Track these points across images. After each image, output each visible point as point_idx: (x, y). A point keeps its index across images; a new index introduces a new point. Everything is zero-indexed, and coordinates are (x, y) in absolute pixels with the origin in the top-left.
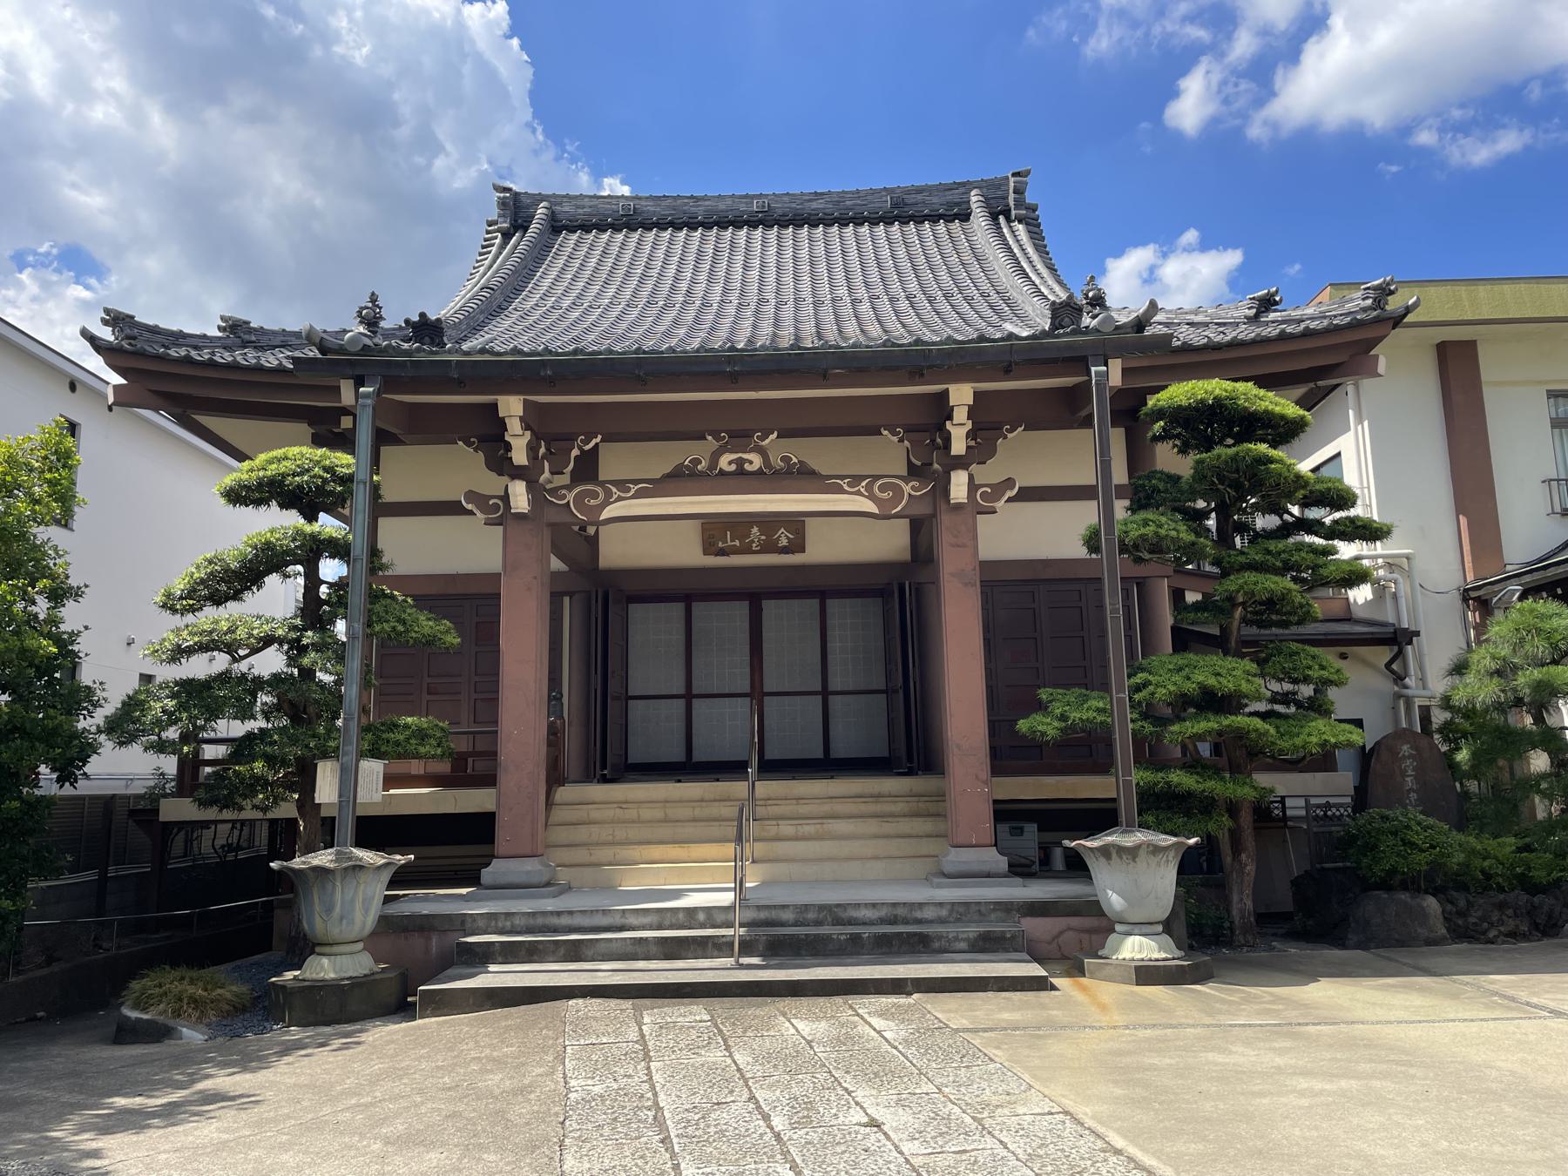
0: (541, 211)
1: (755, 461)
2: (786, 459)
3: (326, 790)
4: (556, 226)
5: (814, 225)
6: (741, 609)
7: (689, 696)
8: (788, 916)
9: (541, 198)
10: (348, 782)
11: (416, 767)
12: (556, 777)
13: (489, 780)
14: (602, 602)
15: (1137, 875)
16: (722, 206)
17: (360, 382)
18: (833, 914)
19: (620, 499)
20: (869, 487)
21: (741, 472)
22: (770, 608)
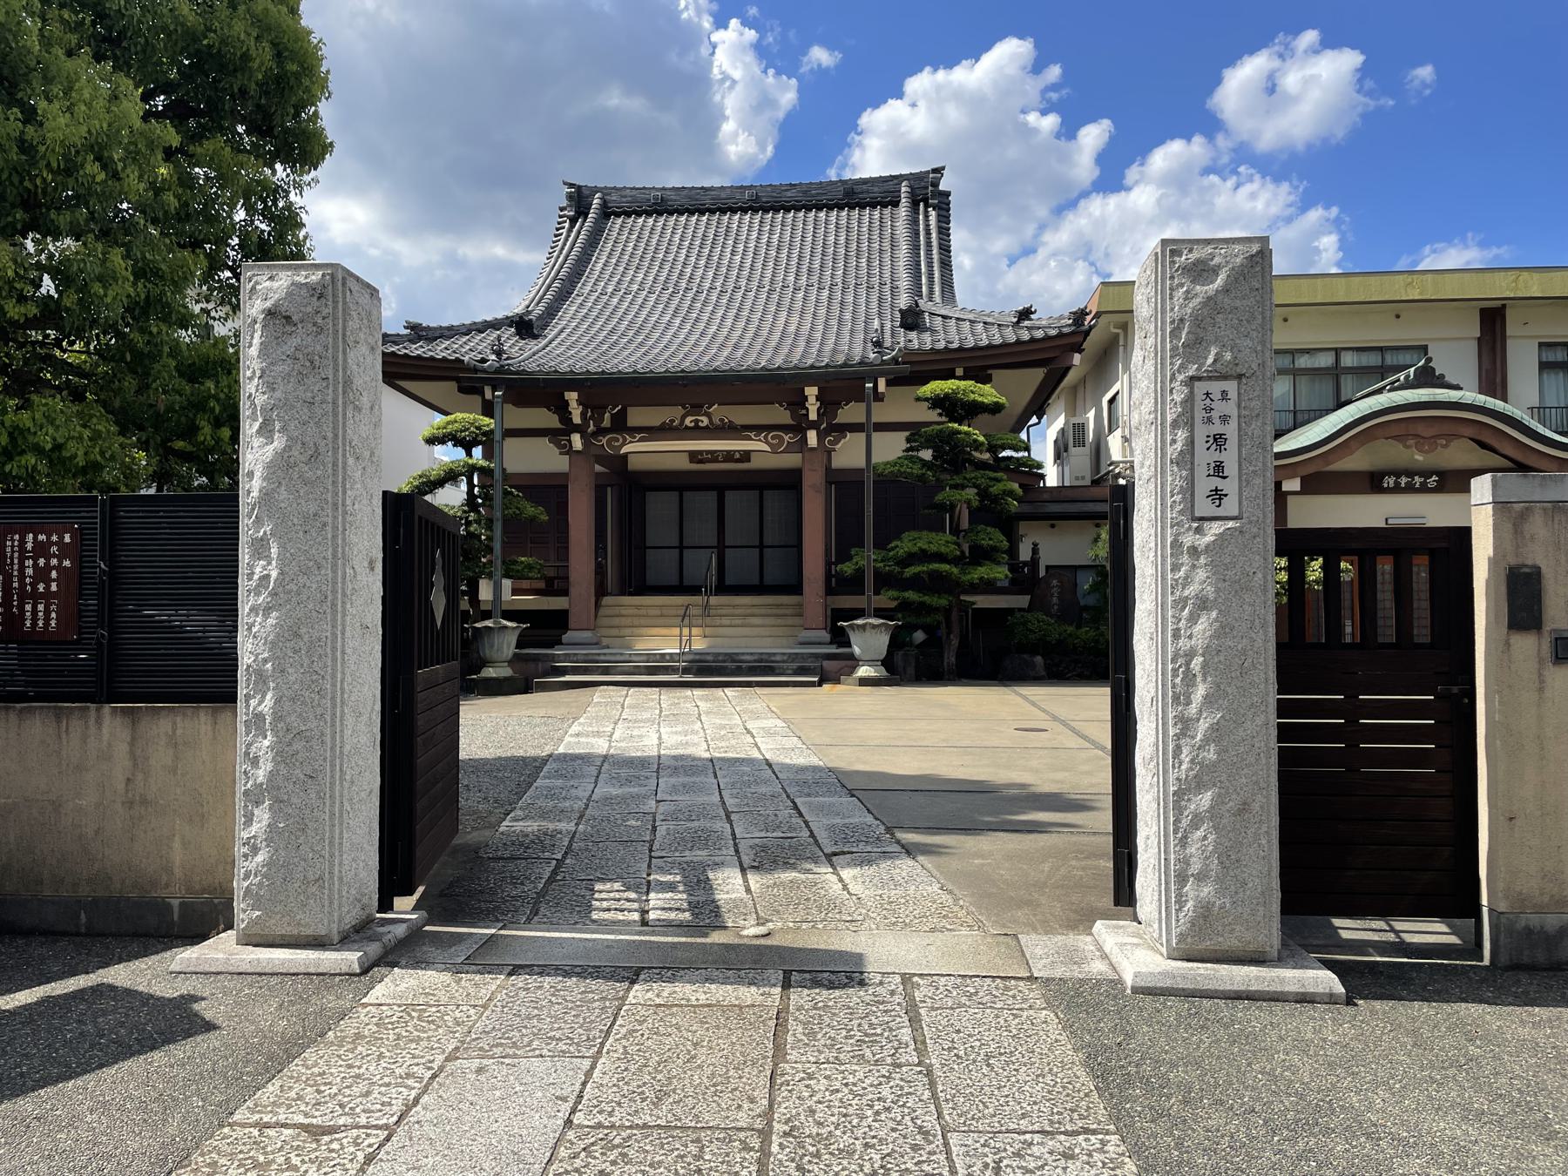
1: (705, 421)
3: (485, 592)
4: (607, 213)
5: (788, 210)
6: (711, 497)
7: (681, 548)
8: (710, 658)
9: (595, 190)
10: (497, 590)
11: (525, 584)
12: (601, 591)
13: (565, 593)
14: (629, 490)
15: (870, 640)
16: (723, 195)
17: (494, 389)
18: (731, 657)
21: (697, 427)
22: (730, 496)
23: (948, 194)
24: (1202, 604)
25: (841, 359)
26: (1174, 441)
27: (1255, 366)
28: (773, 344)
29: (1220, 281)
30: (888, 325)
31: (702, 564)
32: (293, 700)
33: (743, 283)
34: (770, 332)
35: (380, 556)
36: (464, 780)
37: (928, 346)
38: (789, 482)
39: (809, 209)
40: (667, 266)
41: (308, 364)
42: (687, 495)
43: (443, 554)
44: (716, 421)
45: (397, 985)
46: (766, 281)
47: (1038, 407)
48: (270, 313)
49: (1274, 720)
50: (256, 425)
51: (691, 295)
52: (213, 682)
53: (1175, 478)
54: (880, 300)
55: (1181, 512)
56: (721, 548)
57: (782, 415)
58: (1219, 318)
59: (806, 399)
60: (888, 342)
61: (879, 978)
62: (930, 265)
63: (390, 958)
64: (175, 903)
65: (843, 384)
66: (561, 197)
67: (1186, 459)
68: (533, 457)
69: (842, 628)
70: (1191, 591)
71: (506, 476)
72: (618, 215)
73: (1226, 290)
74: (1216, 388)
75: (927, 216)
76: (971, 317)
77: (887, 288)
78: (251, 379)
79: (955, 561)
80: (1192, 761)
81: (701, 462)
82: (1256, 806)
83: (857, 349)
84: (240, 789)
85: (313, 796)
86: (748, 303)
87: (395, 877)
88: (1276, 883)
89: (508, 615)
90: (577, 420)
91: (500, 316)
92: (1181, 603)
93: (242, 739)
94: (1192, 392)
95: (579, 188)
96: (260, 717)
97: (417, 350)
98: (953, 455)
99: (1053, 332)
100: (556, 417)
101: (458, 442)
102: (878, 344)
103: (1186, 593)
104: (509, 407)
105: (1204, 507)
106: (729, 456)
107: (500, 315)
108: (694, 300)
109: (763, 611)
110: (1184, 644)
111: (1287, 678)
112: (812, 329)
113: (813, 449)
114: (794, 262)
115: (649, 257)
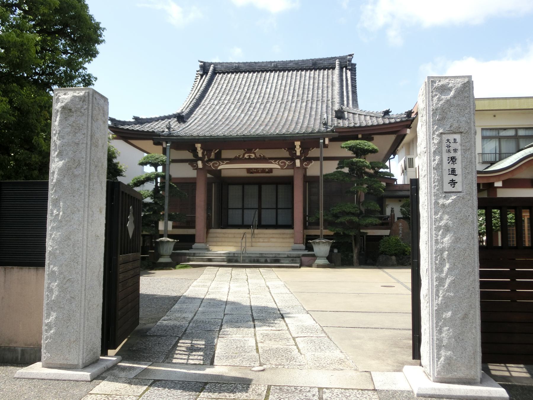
0: (211, 68)
1: (253, 156)
2: (260, 155)
3: (161, 226)
4: (215, 73)
5: (289, 71)
6: (256, 187)
9: (211, 63)
10: (166, 226)
12: (209, 226)
14: (221, 185)
15: (322, 249)
16: (263, 65)
17: (167, 143)
21: (250, 158)
22: (264, 187)
23: (355, 65)
24: (447, 229)
25: (310, 130)
26: (434, 160)
27: (467, 128)
28: (282, 124)
29: (452, 93)
30: (330, 117)
31: (251, 216)
32: (66, 265)
33: (270, 100)
34: (281, 120)
35: (105, 207)
36: (141, 300)
37: (347, 125)
38: (288, 182)
39: (298, 70)
40: (239, 94)
41: (76, 129)
42: (246, 187)
43: (133, 208)
44: (258, 156)
45: (105, 386)
46: (280, 99)
47: (393, 151)
48: (63, 108)
49: (477, 279)
50: (56, 153)
51: (249, 105)
52: (34, 258)
53: (434, 176)
54: (327, 106)
55: (438, 190)
56: (260, 209)
57: (285, 153)
58: (452, 109)
60: (330, 123)
61: (308, 389)
62: (347, 92)
63: (104, 375)
64: (19, 349)
65: (310, 141)
66: (197, 67)
67: (439, 167)
68: (183, 171)
69: (310, 243)
70: (442, 223)
72: (220, 73)
73: (454, 97)
74: (451, 137)
75: (346, 74)
76: (364, 113)
77: (330, 101)
78: (55, 134)
79: (358, 215)
80: (443, 297)
81: (252, 173)
82: (470, 316)
83: (317, 127)
84: (45, 302)
85: (74, 306)
86: (272, 108)
87: (108, 343)
88: (479, 349)
89: (170, 236)
90: (200, 155)
91: (171, 114)
92: (438, 228)
93: (46, 281)
94: (441, 139)
95: (204, 63)
96: (53, 272)
97: (137, 127)
98: (357, 170)
99: (398, 120)
101: (152, 164)
102: (325, 124)
103: (440, 224)
104: (173, 151)
105: (448, 187)
106: (263, 170)
107: (171, 114)
108: (250, 107)
109: (277, 236)
110: (440, 246)
111: (484, 261)
112: (298, 118)
113: (298, 168)
114: (292, 91)
115: (232, 90)
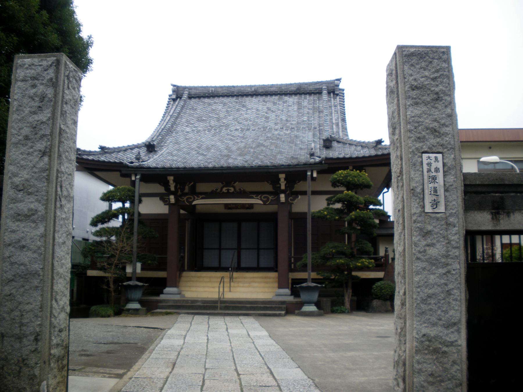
3: (129, 270)
7: (220, 249)
14: (200, 220)
19: (197, 199)
20: (261, 197)
38: (271, 219)
59: (279, 179)
65: (296, 174)
68: (151, 207)
69: (296, 287)
71: (139, 214)
81: (230, 208)
83: (303, 157)
90: (172, 189)
100: (163, 188)
106: (243, 206)
113: (283, 203)
